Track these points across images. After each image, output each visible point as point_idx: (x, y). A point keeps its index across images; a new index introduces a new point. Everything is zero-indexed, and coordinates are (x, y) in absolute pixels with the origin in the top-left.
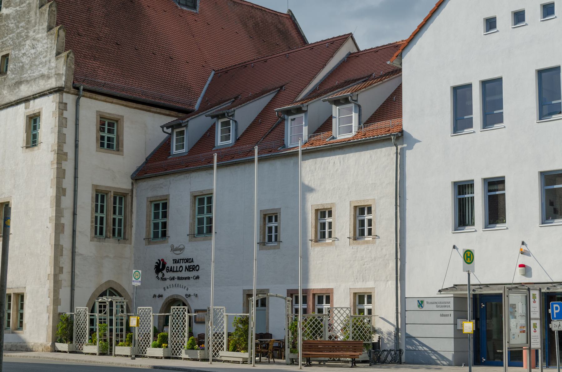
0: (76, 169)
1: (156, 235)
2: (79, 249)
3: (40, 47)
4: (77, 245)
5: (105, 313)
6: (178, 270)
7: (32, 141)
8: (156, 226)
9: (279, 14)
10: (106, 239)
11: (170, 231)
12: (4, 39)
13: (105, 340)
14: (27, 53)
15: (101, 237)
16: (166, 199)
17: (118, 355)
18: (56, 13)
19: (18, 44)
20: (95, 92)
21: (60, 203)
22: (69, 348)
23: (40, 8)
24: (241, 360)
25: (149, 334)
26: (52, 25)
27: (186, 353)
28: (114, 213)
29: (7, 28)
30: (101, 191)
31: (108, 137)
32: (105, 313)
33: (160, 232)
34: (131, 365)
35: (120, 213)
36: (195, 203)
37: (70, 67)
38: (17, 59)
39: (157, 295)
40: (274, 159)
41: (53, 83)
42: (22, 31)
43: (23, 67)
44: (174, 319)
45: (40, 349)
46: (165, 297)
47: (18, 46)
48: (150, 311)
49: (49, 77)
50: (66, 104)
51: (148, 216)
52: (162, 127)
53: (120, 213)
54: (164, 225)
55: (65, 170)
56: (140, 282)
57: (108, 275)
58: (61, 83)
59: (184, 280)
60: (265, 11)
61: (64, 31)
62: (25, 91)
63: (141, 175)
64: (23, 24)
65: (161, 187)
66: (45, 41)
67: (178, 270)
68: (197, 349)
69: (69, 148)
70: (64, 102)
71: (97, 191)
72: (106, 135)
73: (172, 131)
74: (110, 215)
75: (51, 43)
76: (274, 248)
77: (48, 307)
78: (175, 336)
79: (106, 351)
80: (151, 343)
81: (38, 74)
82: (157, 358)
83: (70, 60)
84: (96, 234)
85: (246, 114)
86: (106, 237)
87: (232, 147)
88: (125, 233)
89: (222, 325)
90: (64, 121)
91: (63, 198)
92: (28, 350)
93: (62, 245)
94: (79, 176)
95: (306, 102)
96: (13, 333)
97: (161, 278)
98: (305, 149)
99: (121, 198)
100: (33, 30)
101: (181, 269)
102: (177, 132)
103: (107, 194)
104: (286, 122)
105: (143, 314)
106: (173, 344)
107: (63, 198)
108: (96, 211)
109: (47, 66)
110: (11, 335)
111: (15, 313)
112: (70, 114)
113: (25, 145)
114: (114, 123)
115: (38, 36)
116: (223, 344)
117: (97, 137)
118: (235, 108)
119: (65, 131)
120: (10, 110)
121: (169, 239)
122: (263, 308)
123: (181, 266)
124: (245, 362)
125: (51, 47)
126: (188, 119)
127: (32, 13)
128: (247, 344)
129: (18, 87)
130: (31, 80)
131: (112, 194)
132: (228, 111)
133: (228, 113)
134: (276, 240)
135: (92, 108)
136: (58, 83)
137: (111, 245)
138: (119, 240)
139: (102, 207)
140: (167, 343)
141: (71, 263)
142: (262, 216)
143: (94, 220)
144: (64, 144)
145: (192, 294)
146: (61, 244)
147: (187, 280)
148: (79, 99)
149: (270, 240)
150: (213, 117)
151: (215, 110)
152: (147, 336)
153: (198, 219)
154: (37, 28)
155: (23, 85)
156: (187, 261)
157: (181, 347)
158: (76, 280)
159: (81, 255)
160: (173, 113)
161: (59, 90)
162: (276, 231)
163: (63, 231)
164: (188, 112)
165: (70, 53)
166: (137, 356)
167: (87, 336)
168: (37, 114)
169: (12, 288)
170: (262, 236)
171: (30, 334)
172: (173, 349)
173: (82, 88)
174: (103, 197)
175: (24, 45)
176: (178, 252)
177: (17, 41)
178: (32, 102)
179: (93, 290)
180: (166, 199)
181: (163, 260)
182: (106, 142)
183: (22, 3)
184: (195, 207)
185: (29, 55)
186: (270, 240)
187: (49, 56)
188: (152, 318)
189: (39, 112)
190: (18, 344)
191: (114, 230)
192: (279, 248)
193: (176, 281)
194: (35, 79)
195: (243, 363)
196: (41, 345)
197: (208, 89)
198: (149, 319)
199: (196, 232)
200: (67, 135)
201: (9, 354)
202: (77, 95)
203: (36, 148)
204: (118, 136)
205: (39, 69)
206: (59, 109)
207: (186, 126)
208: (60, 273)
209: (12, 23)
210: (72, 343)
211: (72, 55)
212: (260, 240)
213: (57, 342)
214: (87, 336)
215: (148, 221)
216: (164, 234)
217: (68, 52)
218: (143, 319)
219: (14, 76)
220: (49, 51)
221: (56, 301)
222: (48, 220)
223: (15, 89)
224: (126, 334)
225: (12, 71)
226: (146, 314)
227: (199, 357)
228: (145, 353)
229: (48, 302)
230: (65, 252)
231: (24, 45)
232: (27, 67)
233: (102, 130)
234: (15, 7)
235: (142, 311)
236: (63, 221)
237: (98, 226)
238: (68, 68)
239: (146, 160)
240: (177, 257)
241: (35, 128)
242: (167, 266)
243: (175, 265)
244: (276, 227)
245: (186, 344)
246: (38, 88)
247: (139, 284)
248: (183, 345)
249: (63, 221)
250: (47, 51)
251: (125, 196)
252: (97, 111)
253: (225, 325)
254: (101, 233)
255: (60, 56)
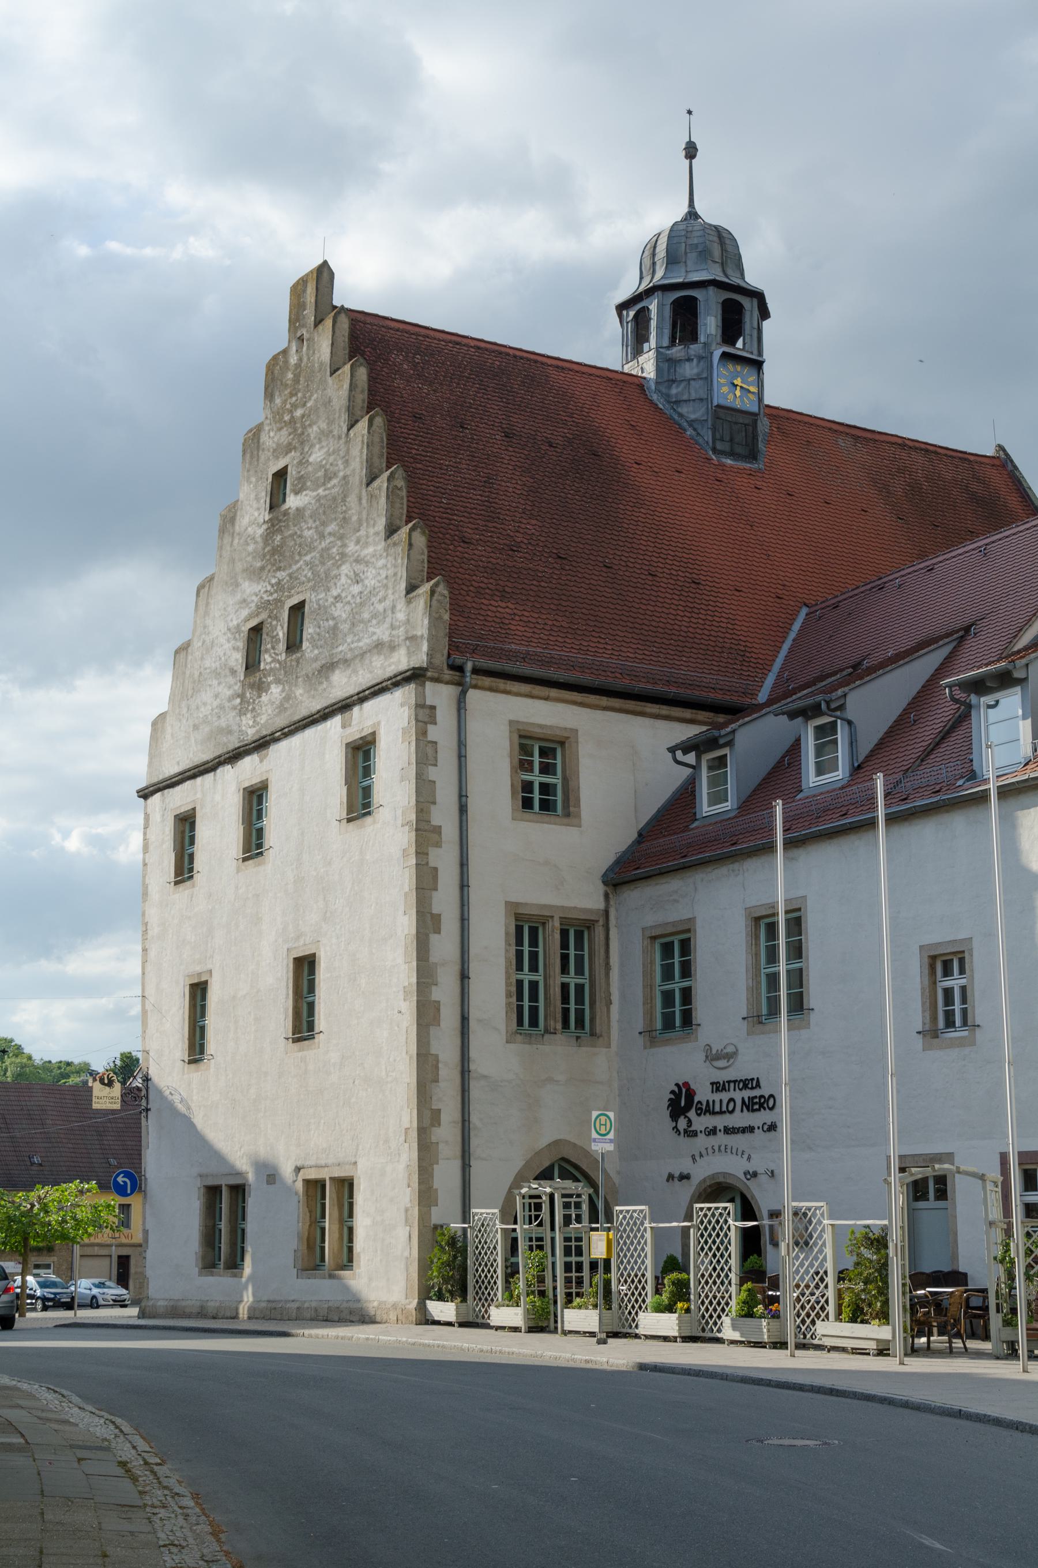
0: (463, 864)
1: (668, 1024)
2: (479, 1063)
3: (371, 578)
4: (473, 1053)
5: (540, 1225)
6: (724, 1108)
7: (360, 803)
8: (668, 998)
9: (972, 458)
10: (547, 1036)
11: (701, 1011)
12: (295, 568)
13: (542, 1294)
14: (343, 595)
15: (533, 1031)
16: (689, 931)
17: (570, 1332)
18: (404, 493)
19: (323, 575)
20: (501, 677)
21: (427, 951)
22: (458, 1314)
23: (368, 485)
24: (872, 1345)
25: (643, 1275)
26: (398, 522)
27: (734, 1327)
28: (565, 970)
29: (298, 541)
30: (529, 918)
31: (541, 784)
32: (540, 1225)
33: (676, 1015)
34: (587, 1361)
35: (580, 971)
36: (757, 937)
37: (440, 618)
38: (322, 611)
39: (677, 1175)
40: (948, 811)
41: (401, 661)
42: (332, 544)
43: (335, 628)
44: (702, 1236)
45: (393, 1317)
46: (696, 1180)
47: (323, 581)
48: (645, 1217)
49: (393, 648)
50: (433, 708)
51: (648, 974)
52: (672, 750)
53: (580, 971)
54: (687, 995)
55: (436, 869)
56: (611, 1141)
57: (552, 1128)
58: (420, 659)
59: (740, 1136)
60: (936, 453)
61: (423, 533)
62: (342, 684)
63: (624, 874)
64: (332, 527)
65: (677, 901)
66: (381, 563)
67: (724, 1108)
68: (761, 1317)
69: (444, 815)
70: (428, 703)
71: (518, 917)
72: (537, 778)
73: (698, 758)
74: (555, 977)
75: (395, 566)
76: (961, 1043)
77: (407, 1210)
78: (707, 1283)
79: (542, 1323)
80: (648, 1300)
81: (368, 641)
82: (666, 1339)
83: (438, 601)
84: (520, 1022)
85: (874, 704)
86: (547, 1031)
87: (843, 788)
88: (592, 1020)
89: (821, 1251)
90: (430, 750)
91: (434, 938)
92: (363, 1317)
93: (437, 1056)
94: (472, 882)
95: (1022, 657)
96: (331, 1276)
97: (685, 1131)
98: (1026, 777)
99: (579, 933)
100: (354, 538)
101: (730, 1108)
102: (708, 761)
103: (544, 924)
104: (973, 713)
105: (628, 1224)
106: (703, 1303)
107: (434, 938)
108: (519, 967)
109: (388, 620)
110: (327, 1282)
111: (336, 1227)
112: (443, 732)
113: (344, 815)
114: (554, 750)
115: (366, 552)
116: (827, 1302)
117: (512, 785)
118: (846, 689)
119: (432, 773)
120: (310, 733)
121: (700, 1029)
122: (941, 1204)
123: (732, 1100)
124: (883, 1351)
125: (395, 574)
126: (733, 726)
127: (352, 499)
128: (886, 1303)
129: (327, 678)
130: (354, 658)
131: (557, 924)
132: (827, 697)
133: (828, 703)
134: (965, 1023)
135: (499, 714)
136: (414, 658)
137: (558, 1052)
138: (578, 1038)
139: (534, 956)
140: (688, 1300)
141: (459, 1098)
142: (926, 960)
143: (514, 989)
144: (433, 807)
145: (760, 1170)
146: (433, 1052)
147: (747, 1135)
148: (464, 693)
149: (950, 1023)
150: (792, 715)
151: (796, 701)
152: (640, 1282)
153: (768, 975)
154: (362, 533)
155: (337, 672)
156: (745, 1087)
157: (723, 1310)
158: (474, 1142)
159: (485, 1077)
160: (702, 715)
161: (415, 676)
162: (964, 1000)
163: (436, 1021)
164: (734, 711)
165: (436, 585)
166: (616, 1335)
167: (499, 1283)
168: (370, 738)
169: (326, 1166)
170: (927, 1014)
171: (370, 1279)
172: (703, 1317)
173: (469, 666)
174: (534, 932)
175: (336, 577)
176: (722, 1063)
177: (321, 569)
178: (356, 709)
179: (518, 1164)
180: (689, 931)
181: (686, 1084)
182: (536, 796)
183: (330, 479)
184: (757, 945)
185: (349, 598)
186: (950, 1023)
187: (391, 597)
188: (648, 1235)
189: (374, 734)
190: (345, 1305)
191: (566, 1012)
192: (973, 1043)
193: (722, 1139)
194: (363, 655)
195: (878, 1355)
196: (395, 1306)
197: (791, 650)
198: (642, 1236)
199: (764, 1011)
200: (438, 785)
201: (314, 1332)
202: (459, 684)
203: (368, 820)
204: (565, 780)
205: (371, 629)
206: (417, 720)
207: (730, 744)
208: (433, 1126)
209: (309, 529)
210: (464, 1300)
211: (442, 589)
212: (924, 1024)
213: (431, 1299)
214: (499, 1283)
215: (649, 987)
216: (687, 1019)
217: (432, 582)
218: (628, 1237)
219: (316, 652)
220: (390, 585)
221: (426, 1196)
222: (401, 996)
223: (321, 683)
224: (584, 1277)
225: (312, 640)
226: (635, 1224)
227: (766, 1338)
228: (637, 1327)
229: (408, 1199)
230: (443, 1072)
231: (338, 576)
232: (345, 627)
233: (525, 765)
234: (313, 490)
235: (624, 1218)
236: (436, 994)
237: (526, 1003)
238: (434, 621)
239: (640, 834)
240: (722, 1077)
241: (367, 772)
242: (696, 1099)
243: (717, 1097)
244: (963, 989)
245: (733, 1303)
246: (369, 675)
247: (610, 1147)
248: (727, 1304)
249: (436, 994)
250: (386, 586)
251: (588, 928)
252: (511, 722)
253: (829, 1251)
254: (534, 1022)
255: (414, 594)
